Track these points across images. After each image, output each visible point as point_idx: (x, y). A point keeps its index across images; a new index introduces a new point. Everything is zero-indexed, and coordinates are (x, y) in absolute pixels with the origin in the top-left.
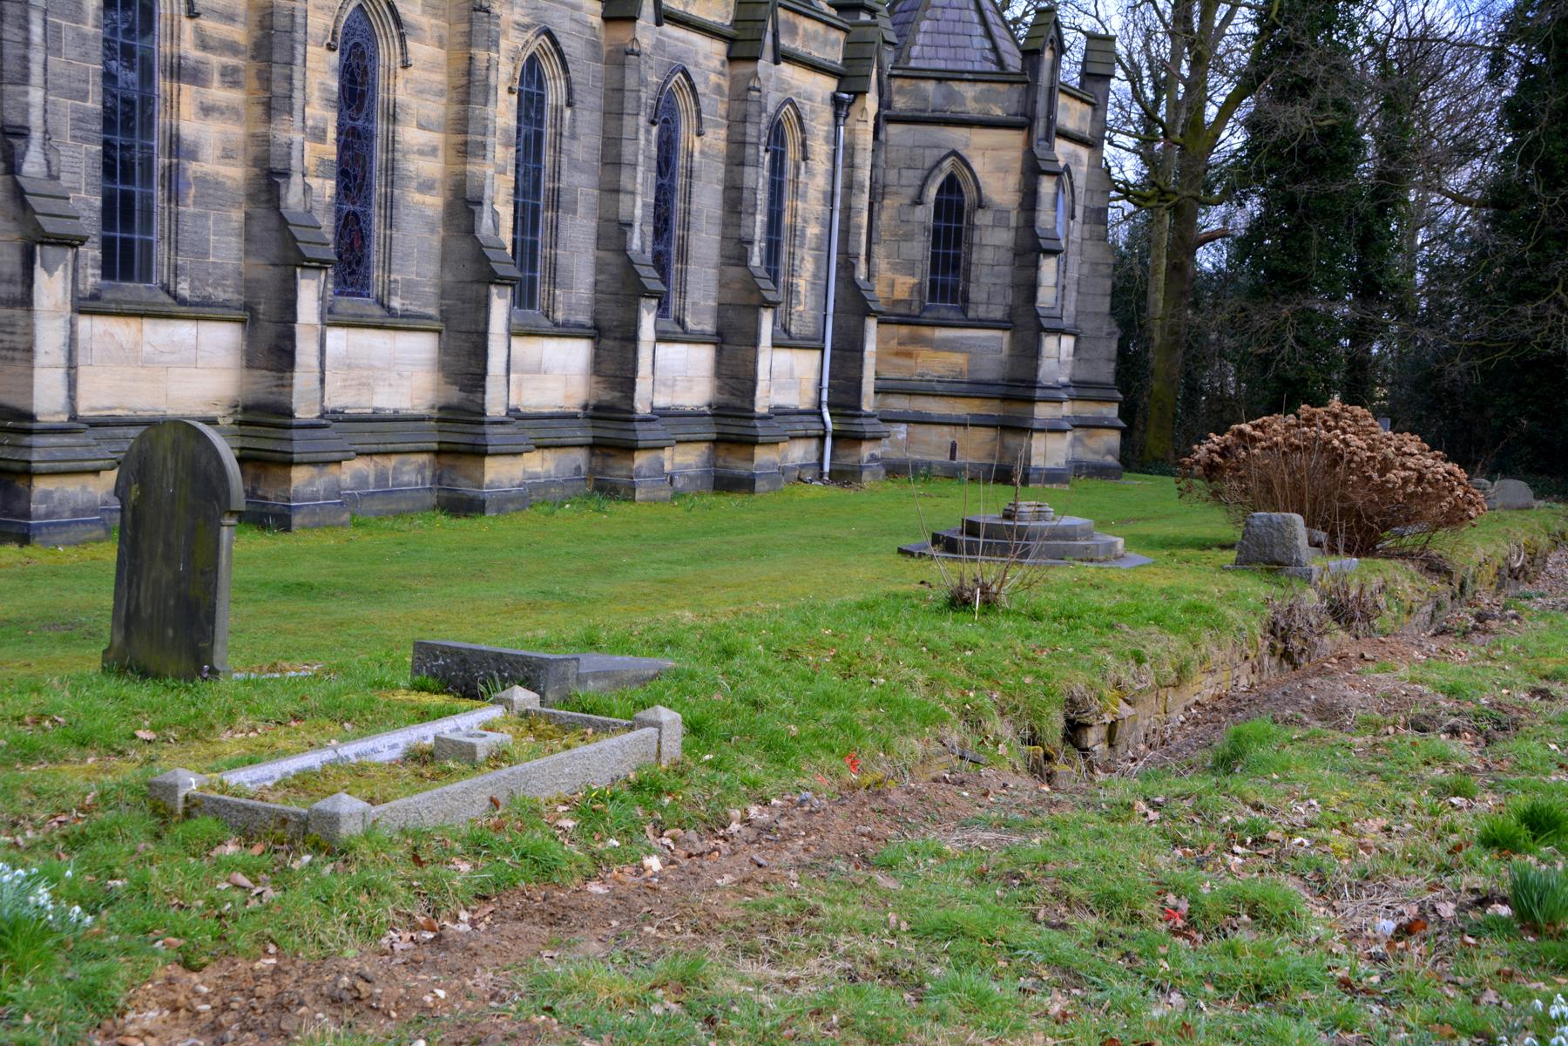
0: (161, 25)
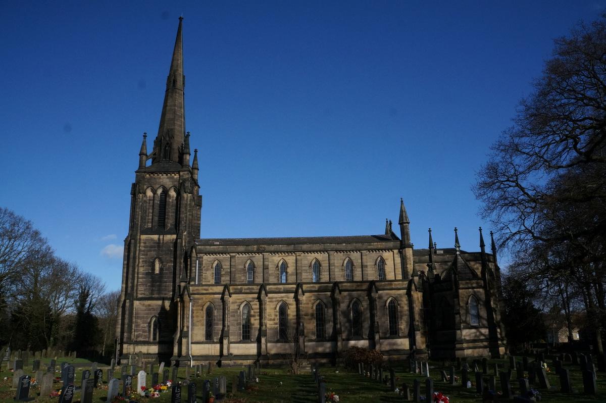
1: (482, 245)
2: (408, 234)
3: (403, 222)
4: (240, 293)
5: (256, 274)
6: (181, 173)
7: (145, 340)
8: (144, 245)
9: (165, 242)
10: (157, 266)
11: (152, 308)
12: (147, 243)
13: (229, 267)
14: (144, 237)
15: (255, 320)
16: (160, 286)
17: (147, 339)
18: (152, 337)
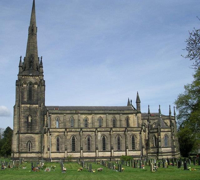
1: (170, 113)
2: (140, 107)
3: (138, 101)
6: (39, 76)
10: (30, 119)
14: (23, 105)
16: (31, 128)
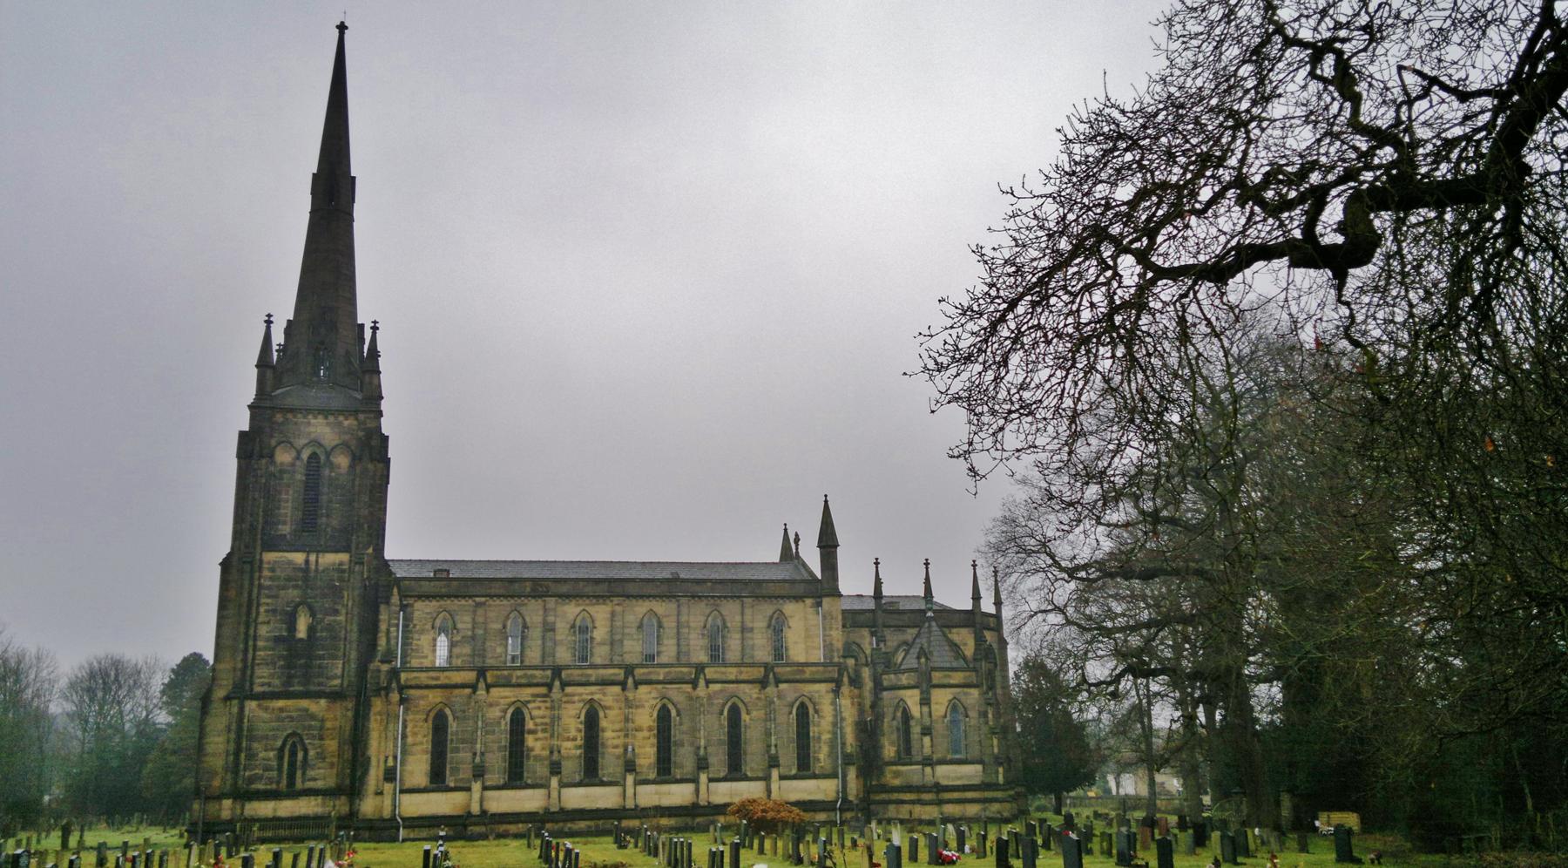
0: (811, 717)
1: (976, 597)
4: (508, 685)
5: (528, 643)
7: (269, 787)
8: (270, 574)
9: (321, 568)
11: (288, 717)
12: (278, 570)
13: (470, 626)
15: (537, 740)
16: (308, 666)
17: (274, 786)
18: (284, 782)
